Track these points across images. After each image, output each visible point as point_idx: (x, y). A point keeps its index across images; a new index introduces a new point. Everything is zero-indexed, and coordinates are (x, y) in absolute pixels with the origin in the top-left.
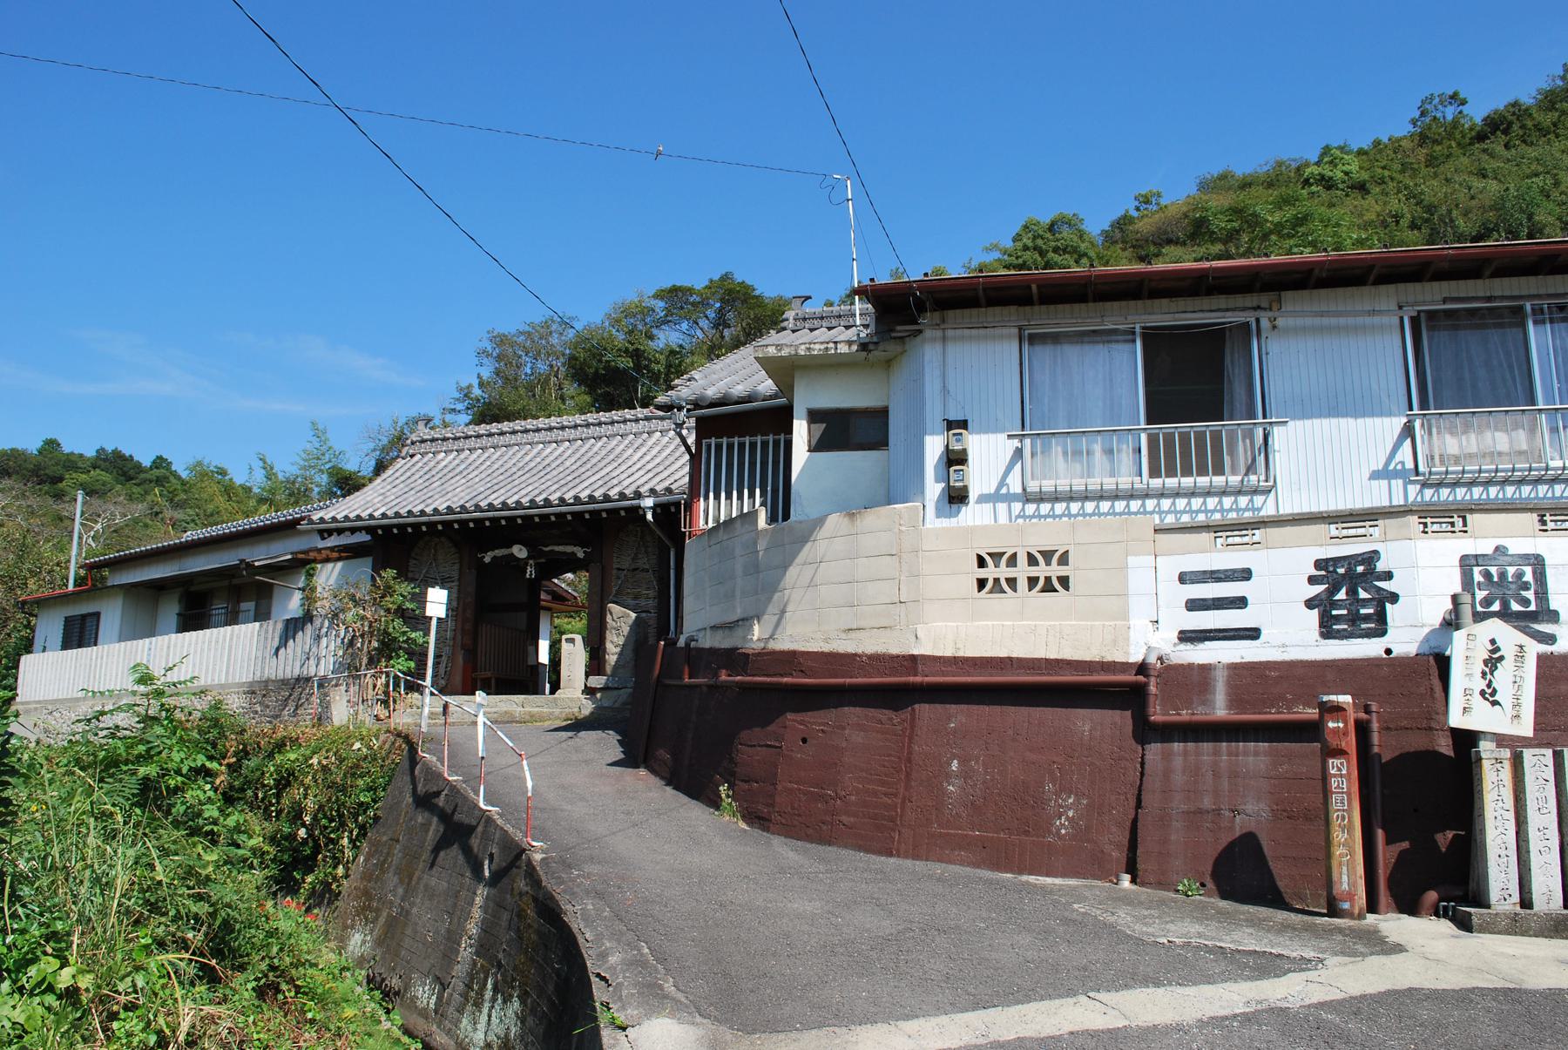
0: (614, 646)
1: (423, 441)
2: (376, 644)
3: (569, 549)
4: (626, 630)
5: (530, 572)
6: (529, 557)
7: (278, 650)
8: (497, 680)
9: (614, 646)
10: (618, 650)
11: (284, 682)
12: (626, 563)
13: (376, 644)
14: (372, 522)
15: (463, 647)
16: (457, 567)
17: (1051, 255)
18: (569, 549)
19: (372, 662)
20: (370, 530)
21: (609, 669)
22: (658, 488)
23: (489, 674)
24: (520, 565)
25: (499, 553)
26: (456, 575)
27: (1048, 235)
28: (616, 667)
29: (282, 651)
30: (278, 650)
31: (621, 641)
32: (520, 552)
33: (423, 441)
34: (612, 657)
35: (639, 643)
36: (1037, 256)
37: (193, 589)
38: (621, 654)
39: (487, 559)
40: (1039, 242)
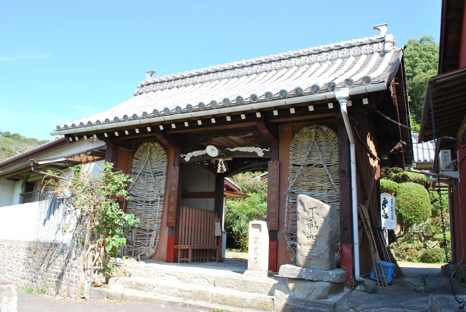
0: (308, 234)
1: (149, 84)
2: (97, 223)
3: (251, 149)
4: (320, 221)
5: (222, 167)
6: (219, 156)
7: (45, 221)
8: (193, 250)
9: (308, 234)
10: (311, 241)
11: (45, 244)
12: (302, 159)
13: (97, 223)
14: (99, 127)
15: (168, 224)
16: (165, 164)
17: (422, 52)
18: (251, 149)
19: (93, 238)
20: (100, 134)
21: (301, 259)
22: (355, 79)
23: (186, 247)
24: (210, 164)
25: (196, 153)
26: (164, 170)
27: (420, 44)
28: (309, 258)
29: (47, 222)
30: (45, 221)
31: (315, 232)
32: (212, 151)
33: (149, 84)
34: (305, 245)
35: (338, 235)
36: (416, 52)
37: (29, 180)
38: (314, 246)
39: (187, 159)
40: (417, 47)
